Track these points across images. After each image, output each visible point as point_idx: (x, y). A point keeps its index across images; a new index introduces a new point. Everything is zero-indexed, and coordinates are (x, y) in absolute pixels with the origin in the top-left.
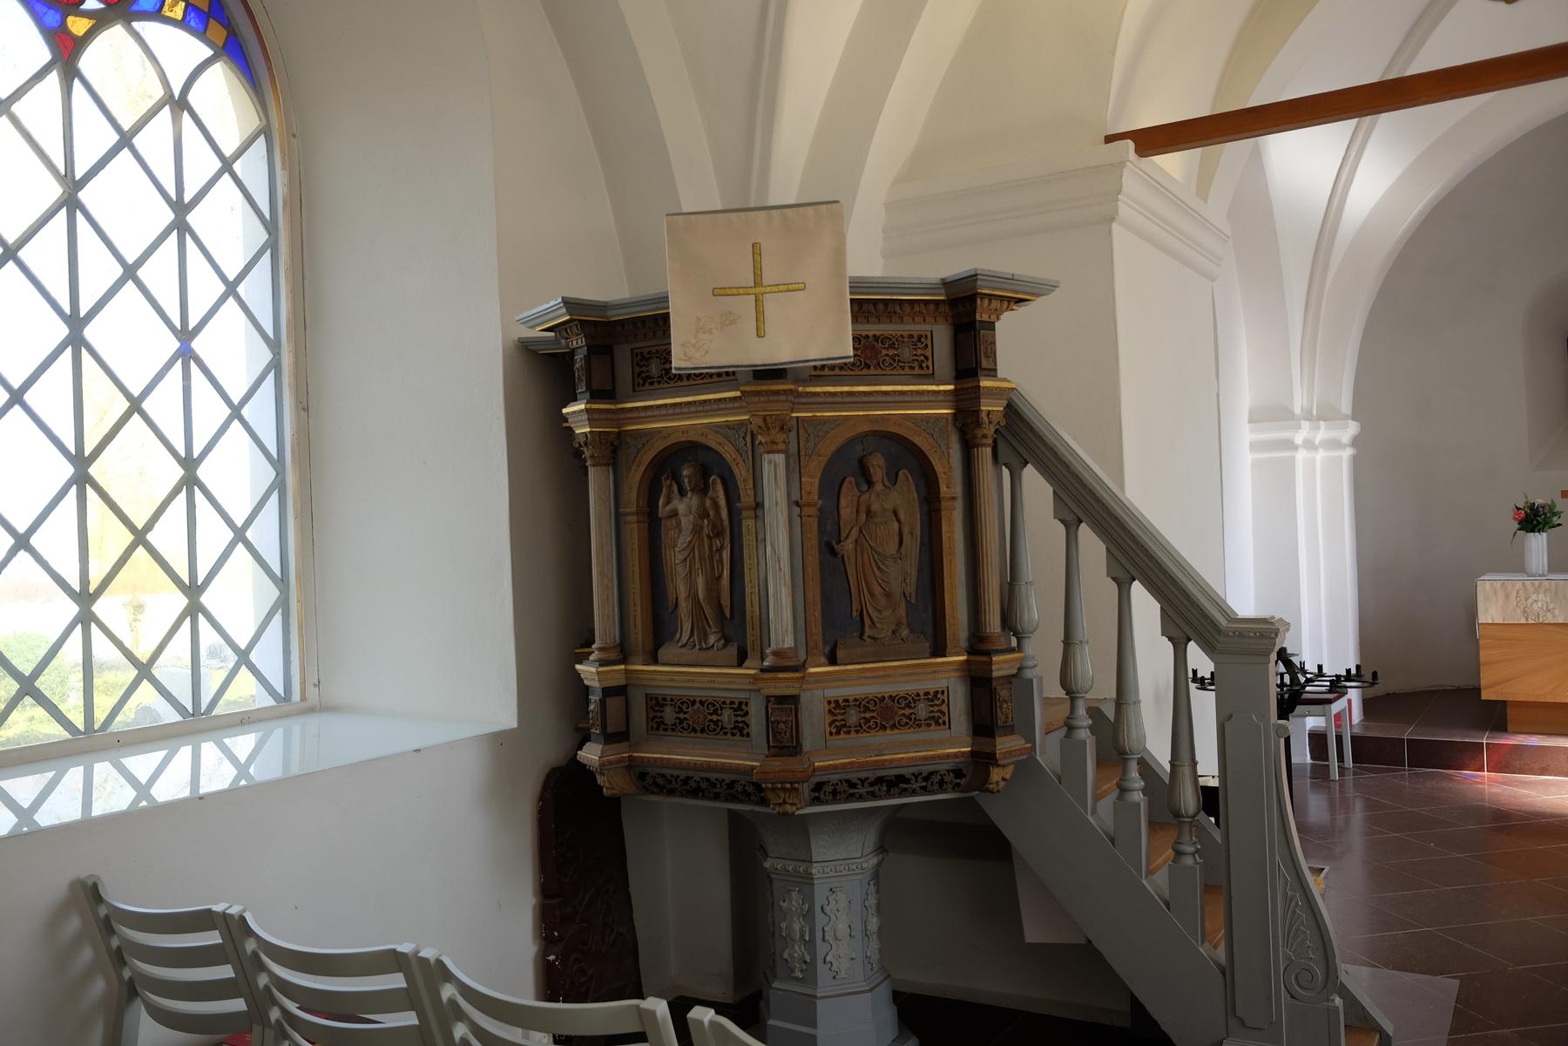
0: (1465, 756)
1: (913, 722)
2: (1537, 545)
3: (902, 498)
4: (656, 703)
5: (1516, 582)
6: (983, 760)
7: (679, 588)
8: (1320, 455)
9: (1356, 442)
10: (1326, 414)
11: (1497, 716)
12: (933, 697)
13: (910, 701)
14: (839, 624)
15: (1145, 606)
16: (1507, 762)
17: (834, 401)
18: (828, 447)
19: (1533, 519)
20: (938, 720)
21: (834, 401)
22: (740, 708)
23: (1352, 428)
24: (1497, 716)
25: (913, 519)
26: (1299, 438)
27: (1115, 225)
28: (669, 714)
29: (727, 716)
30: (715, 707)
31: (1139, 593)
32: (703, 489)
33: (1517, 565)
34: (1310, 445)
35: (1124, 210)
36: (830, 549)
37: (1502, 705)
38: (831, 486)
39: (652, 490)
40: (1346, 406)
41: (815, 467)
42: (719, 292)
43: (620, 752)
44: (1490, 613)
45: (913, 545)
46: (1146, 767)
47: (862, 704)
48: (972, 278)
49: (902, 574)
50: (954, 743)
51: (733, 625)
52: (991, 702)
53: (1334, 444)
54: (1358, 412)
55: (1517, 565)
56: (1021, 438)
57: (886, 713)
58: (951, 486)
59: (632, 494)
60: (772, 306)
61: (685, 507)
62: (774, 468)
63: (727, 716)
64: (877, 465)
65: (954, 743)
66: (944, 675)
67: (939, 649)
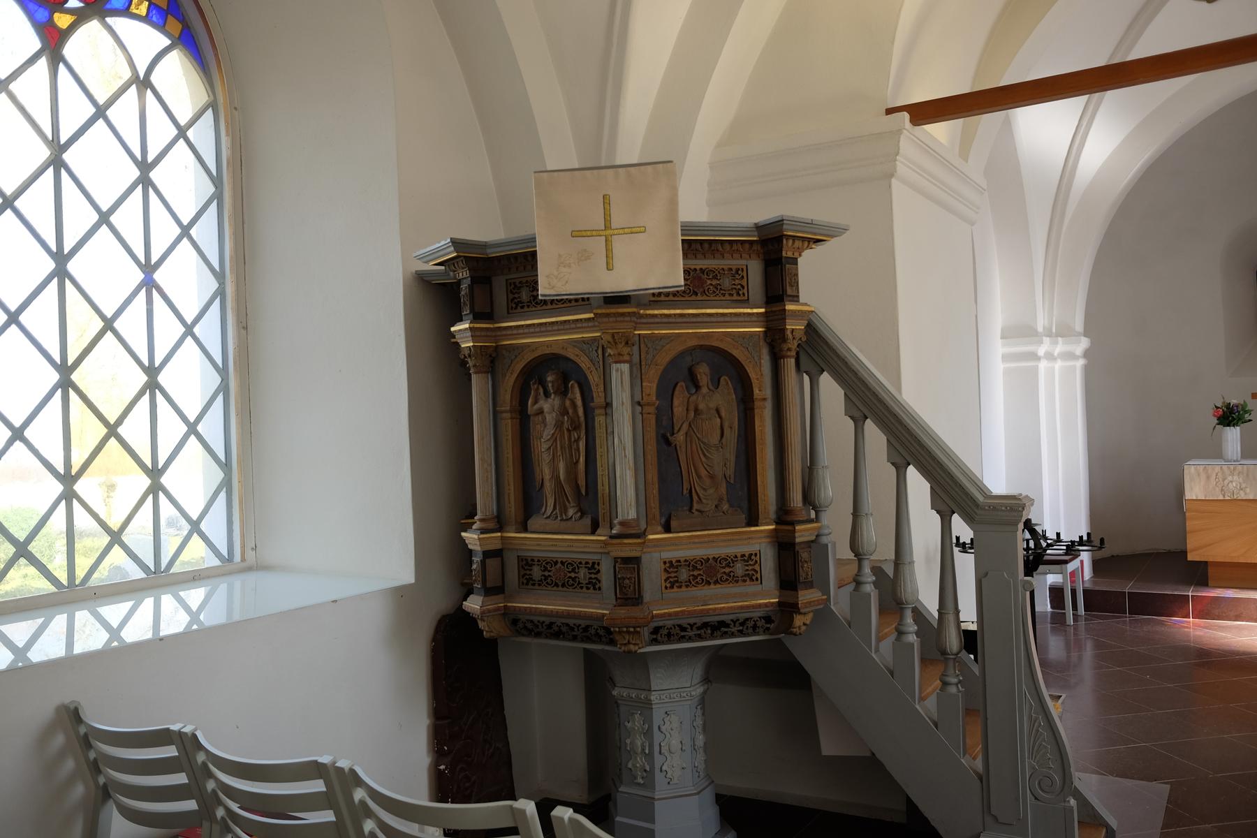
0: (1174, 606)
1: (732, 579)
2: (1232, 436)
3: (723, 399)
4: (526, 563)
5: (1215, 466)
6: (788, 609)
7: (544, 471)
8: (1058, 365)
9: (1087, 354)
10: (1063, 332)
11: (1200, 574)
12: (748, 559)
13: (729, 561)
14: (672, 500)
15: (918, 485)
16: (1208, 610)
17: (668, 321)
18: (664, 358)
19: (1229, 416)
20: (752, 577)
21: (668, 321)
22: (593, 567)
23: (1084, 343)
24: (1200, 574)
25: (732, 416)
26: (1041, 351)
27: (894, 181)
28: (537, 572)
29: (582, 574)
30: (573, 566)
31: (913, 475)
32: (563, 392)
33: (1216, 452)
34: (1050, 356)
35: (901, 168)
36: (665, 440)
37: (1204, 565)
38: (666, 390)
39: (522, 393)
40: (1079, 326)
41: (653, 374)
42: (577, 234)
43: (497, 602)
44: (1194, 491)
45: (732, 436)
46: (919, 615)
47: (691, 564)
48: (779, 223)
49: (723, 460)
50: (765, 595)
51: (588, 500)
52: (794, 563)
53: (1069, 356)
54: (1089, 330)
55: (1216, 452)
56: (819, 351)
57: (710, 571)
58: (763, 389)
59: (506, 396)
60: (619, 245)
61: (549, 406)
62: (620, 375)
63: (582, 574)
64: (703, 373)
65: (765, 595)
66: (757, 541)
67: (753, 520)
